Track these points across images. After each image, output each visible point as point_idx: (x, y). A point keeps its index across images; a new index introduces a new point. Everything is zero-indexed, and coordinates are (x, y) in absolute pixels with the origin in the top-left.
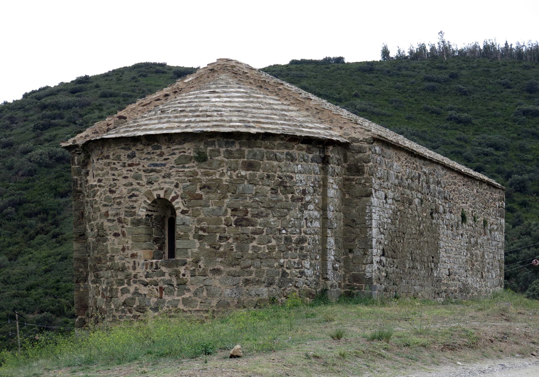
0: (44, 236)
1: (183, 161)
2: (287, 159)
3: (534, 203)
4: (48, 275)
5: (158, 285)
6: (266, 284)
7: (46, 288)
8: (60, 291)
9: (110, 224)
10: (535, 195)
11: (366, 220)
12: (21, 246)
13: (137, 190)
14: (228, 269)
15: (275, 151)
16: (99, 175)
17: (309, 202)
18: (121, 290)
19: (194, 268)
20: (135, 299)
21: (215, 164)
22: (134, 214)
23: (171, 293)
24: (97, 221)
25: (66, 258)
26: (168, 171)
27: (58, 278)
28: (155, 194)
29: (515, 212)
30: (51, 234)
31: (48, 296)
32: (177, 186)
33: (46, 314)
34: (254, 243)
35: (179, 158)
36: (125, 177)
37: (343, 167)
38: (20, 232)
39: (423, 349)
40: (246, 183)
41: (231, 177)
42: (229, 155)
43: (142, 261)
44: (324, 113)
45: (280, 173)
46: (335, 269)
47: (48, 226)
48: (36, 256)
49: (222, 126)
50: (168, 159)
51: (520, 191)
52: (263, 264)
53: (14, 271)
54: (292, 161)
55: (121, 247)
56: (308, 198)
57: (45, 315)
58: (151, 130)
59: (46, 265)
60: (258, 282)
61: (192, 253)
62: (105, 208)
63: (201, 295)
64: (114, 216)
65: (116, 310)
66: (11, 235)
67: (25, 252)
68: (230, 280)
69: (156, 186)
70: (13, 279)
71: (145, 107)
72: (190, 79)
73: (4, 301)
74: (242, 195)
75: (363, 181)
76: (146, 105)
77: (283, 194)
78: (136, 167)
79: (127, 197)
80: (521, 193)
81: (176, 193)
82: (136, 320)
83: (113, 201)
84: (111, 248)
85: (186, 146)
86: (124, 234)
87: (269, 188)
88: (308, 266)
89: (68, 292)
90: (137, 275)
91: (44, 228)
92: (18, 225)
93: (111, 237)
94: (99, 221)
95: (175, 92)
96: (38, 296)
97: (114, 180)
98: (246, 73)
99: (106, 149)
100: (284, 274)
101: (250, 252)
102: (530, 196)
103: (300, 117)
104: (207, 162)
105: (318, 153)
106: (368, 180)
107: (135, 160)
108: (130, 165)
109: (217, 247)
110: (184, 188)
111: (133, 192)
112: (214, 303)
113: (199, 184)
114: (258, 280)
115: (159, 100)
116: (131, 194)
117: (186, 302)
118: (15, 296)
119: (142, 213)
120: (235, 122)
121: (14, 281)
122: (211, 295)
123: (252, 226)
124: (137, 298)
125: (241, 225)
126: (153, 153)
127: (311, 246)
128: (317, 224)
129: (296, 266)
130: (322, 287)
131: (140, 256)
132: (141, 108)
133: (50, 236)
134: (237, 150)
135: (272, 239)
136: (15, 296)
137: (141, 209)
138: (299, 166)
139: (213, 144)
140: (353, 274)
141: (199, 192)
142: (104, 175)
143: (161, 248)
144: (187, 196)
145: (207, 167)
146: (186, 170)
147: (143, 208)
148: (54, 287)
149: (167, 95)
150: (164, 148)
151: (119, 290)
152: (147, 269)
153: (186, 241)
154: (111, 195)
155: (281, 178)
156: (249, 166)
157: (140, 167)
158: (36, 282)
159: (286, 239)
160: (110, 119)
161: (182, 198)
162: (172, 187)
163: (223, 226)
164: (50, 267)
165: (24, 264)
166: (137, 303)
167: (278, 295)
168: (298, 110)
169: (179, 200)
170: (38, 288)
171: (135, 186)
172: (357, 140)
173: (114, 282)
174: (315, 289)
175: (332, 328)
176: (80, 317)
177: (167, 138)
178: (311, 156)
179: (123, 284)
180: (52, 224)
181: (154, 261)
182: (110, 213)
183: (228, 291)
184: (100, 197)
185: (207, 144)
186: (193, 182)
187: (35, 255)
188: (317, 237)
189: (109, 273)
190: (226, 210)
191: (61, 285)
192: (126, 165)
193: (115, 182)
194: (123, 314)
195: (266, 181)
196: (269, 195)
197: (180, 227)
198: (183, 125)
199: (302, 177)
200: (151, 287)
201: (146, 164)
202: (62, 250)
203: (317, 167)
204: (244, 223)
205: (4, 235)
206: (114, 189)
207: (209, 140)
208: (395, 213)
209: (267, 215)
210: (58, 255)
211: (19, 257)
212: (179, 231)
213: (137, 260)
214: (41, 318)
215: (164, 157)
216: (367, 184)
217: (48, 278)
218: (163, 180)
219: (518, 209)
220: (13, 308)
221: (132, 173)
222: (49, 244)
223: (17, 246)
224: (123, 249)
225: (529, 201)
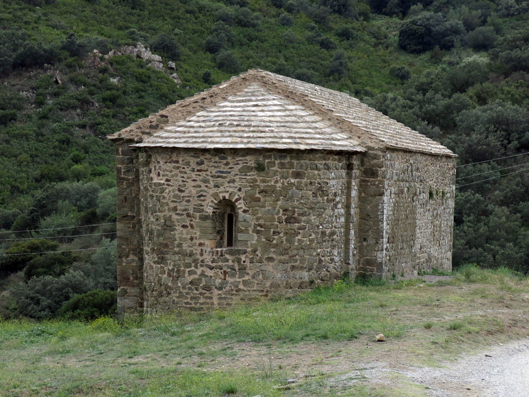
1: (245, 170)
2: (325, 169)
3: (360, 32)
5: (222, 269)
6: (307, 269)
9: (179, 217)
10: (362, 18)
11: (378, 215)
13: (206, 192)
14: (279, 258)
15: (316, 162)
16: (167, 175)
17: (338, 203)
18: (189, 272)
19: (252, 256)
20: (202, 280)
21: (271, 173)
22: (203, 210)
23: (233, 276)
24: (165, 214)
26: (232, 178)
29: (332, 48)
32: (240, 190)
34: (299, 237)
35: (242, 168)
36: (194, 180)
37: (360, 170)
39: (477, 334)
40: (294, 188)
41: (283, 184)
42: (282, 165)
44: (345, 123)
45: (319, 180)
46: (354, 255)
49: (278, 143)
50: (233, 168)
51: (339, 12)
52: (306, 253)
54: (328, 170)
55: (189, 237)
56: (338, 199)
58: (217, 143)
60: (302, 268)
61: (251, 244)
62: (174, 203)
63: (258, 278)
64: (183, 211)
65: (183, 287)
68: (280, 267)
69: (222, 189)
71: (184, 108)
72: (225, 85)
74: (291, 198)
75: (377, 183)
76: (185, 106)
77: (321, 197)
78: (204, 173)
79: (195, 197)
80: (340, 14)
81: (239, 196)
82: (202, 297)
83: (182, 199)
84: (179, 237)
85: (248, 158)
86: (192, 227)
87: (311, 193)
88: (336, 254)
90: (204, 260)
93: (179, 228)
95: (212, 96)
97: (183, 181)
98: (275, 83)
99: (175, 155)
100: (320, 261)
101: (296, 244)
102: (355, 20)
103: (326, 128)
104: (265, 172)
105: (344, 162)
106: (381, 182)
107: (203, 167)
108: (198, 171)
109: (271, 240)
110: (246, 192)
111: (202, 193)
112: (268, 284)
113: (258, 189)
114: (302, 267)
115: (196, 102)
116: (200, 194)
117: (245, 283)
119: (209, 211)
120: (285, 138)
122: (266, 278)
123: (298, 223)
124: (203, 279)
125: (290, 223)
126: (220, 162)
128: (343, 219)
129: (328, 255)
130: (345, 270)
131: (207, 245)
132: (180, 109)
134: (288, 162)
135: (313, 234)
137: (209, 207)
138: (333, 174)
139: (270, 157)
140: (367, 259)
141: (258, 195)
142: (172, 176)
143: (222, 238)
144: (248, 199)
145: (265, 175)
146: (248, 177)
147: (211, 206)
149: (204, 99)
150: (229, 159)
151: (187, 272)
152: (213, 255)
153: (246, 235)
154: (180, 194)
155: (320, 184)
156: (297, 175)
157: (208, 173)
160: (153, 117)
161: (244, 200)
162: (236, 190)
163: (276, 223)
167: (316, 278)
168: (347, 139)
169: (241, 201)
171: (203, 188)
172: (373, 149)
173: (182, 265)
174: (340, 272)
176: (122, 287)
177: (232, 151)
178: (340, 164)
179: (190, 267)
181: (219, 249)
182: (178, 208)
183: (279, 275)
184: (168, 194)
185: (265, 157)
186: (253, 187)
190: (279, 211)
192: (196, 170)
193: (185, 183)
194: (190, 291)
195: (309, 187)
196: (311, 197)
197: (242, 223)
200: (216, 271)
201: (214, 171)
203: (344, 173)
204: (292, 220)
206: (183, 189)
207: (267, 154)
209: (309, 214)
212: (241, 226)
213: (204, 248)
215: (230, 166)
216: (381, 186)
218: (228, 185)
219: (337, 42)
221: (201, 178)
224: (192, 239)
225: (353, 28)
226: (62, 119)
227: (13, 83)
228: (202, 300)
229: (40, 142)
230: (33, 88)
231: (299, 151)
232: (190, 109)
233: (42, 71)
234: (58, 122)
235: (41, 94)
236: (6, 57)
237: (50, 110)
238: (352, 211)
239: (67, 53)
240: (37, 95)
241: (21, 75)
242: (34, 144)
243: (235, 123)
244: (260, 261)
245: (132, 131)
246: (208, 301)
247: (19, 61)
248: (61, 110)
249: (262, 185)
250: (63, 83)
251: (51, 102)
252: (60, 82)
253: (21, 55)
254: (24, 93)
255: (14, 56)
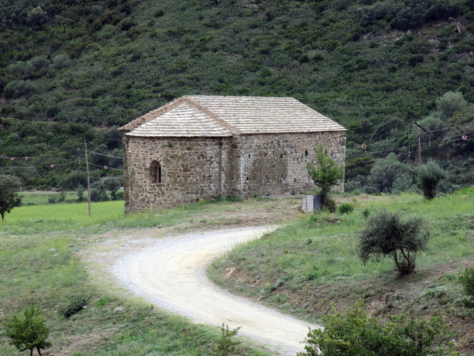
0: (113, 27)
1: (164, 146)
4: (118, 79)
7: (115, 95)
8: (131, 100)
12: (85, 39)
17: (213, 161)
21: (175, 148)
22: (145, 166)
23: (159, 197)
25: (139, 58)
27: (129, 82)
28: (153, 159)
30: (120, 24)
31: (117, 105)
32: (161, 156)
33: (115, 128)
34: (191, 178)
38: (83, 21)
42: (181, 144)
43: (148, 184)
46: (225, 186)
47: (117, 14)
48: (104, 54)
49: (178, 134)
53: (78, 73)
55: (140, 178)
56: (213, 160)
57: (114, 130)
58: (151, 134)
59: (116, 65)
60: (192, 193)
66: (72, 23)
67: (91, 47)
69: (153, 156)
70: (76, 82)
73: (67, 110)
74: (186, 160)
85: (165, 141)
86: (141, 173)
88: (213, 186)
89: (140, 100)
91: (112, 16)
92: (81, 11)
93: (137, 174)
94: (132, 167)
96: (106, 105)
100: (202, 190)
107: (146, 145)
112: (175, 201)
117: (164, 200)
118: (79, 104)
119: (148, 166)
121: (78, 85)
127: (214, 178)
128: (217, 169)
132: (151, 115)
133: (119, 27)
136: (79, 104)
139: (175, 140)
141: (169, 159)
148: (124, 94)
149: (162, 110)
156: (189, 149)
158: (103, 87)
159: (203, 176)
162: (159, 156)
164: (120, 69)
165: (89, 64)
166: (146, 200)
169: (162, 161)
170: (106, 95)
171: (146, 155)
172: (235, 135)
175: (190, 219)
178: (214, 143)
180: (122, 11)
183: (180, 196)
185: (173, 141)
186: (167, 155)
187: (101, 52)
188: (217, 174)
189: (136, 188)
191: (133, 92)
198: (164, 132)
199: (210, 152)
201: (150, 147)
202: (133, 47)
203: (217, 147)
205: (64, 24)
208: (255, 161)
209: (196, 167)
210: (129, 53)
211: (83, 54)
212: (162, 174)
214: (110, 133)
217: (117, 83)
220: (77, 119)
222: (119, 38)
223: (80, 39)
224: (141, 179)
226: (457, 60)
227: (425, 32)
228: (146, 208)
229: (438, 78)
230: (439, 37)
231: (188, 138)
232: (156, 115)
233: (447, 23)
234: (455, 62)
235: (444, 41)
236: (420, 13)
237: (449, 53)
238: (223, 165)
239: (468, 8)
240: (441, 42)
241: (431, 26)
242: (433, 79)
243: (164, 124)
244: (171, 190)
245: (129, 126)
246: (148, 209)
247: (430, 16)
248: (458, 53)
249: (171, 154)
250: (461, 32)
251: (451, 46)
252: (459, 31)
253: (432, 11)
254: (432, 40)
255: (426, 12)
